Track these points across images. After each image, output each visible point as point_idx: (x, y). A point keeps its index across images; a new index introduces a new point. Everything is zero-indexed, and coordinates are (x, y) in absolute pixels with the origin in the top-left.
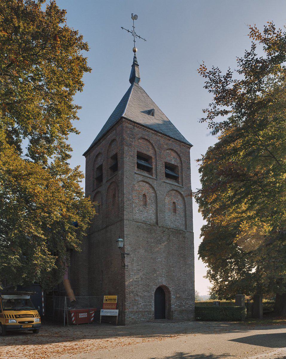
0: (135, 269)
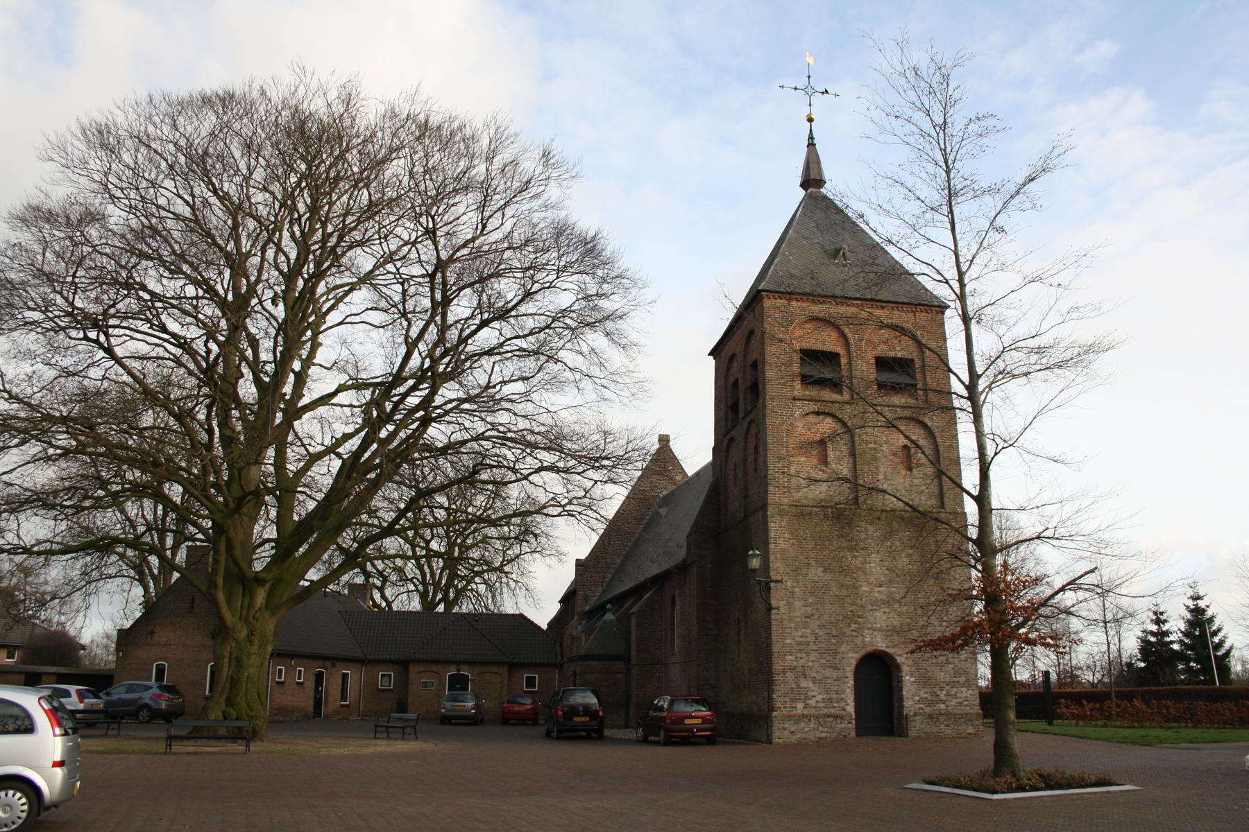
0: (799, 614)
